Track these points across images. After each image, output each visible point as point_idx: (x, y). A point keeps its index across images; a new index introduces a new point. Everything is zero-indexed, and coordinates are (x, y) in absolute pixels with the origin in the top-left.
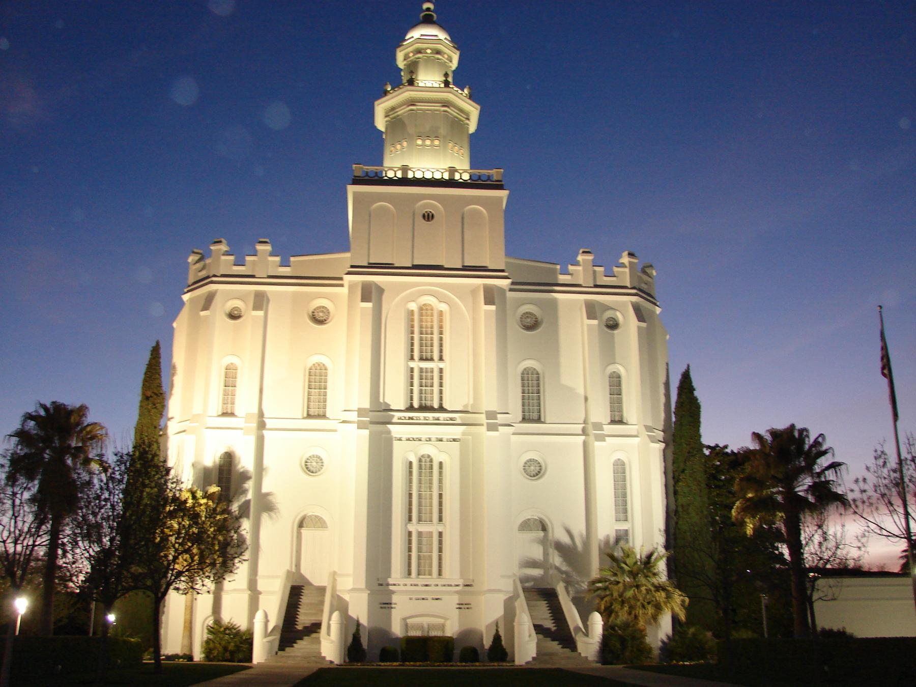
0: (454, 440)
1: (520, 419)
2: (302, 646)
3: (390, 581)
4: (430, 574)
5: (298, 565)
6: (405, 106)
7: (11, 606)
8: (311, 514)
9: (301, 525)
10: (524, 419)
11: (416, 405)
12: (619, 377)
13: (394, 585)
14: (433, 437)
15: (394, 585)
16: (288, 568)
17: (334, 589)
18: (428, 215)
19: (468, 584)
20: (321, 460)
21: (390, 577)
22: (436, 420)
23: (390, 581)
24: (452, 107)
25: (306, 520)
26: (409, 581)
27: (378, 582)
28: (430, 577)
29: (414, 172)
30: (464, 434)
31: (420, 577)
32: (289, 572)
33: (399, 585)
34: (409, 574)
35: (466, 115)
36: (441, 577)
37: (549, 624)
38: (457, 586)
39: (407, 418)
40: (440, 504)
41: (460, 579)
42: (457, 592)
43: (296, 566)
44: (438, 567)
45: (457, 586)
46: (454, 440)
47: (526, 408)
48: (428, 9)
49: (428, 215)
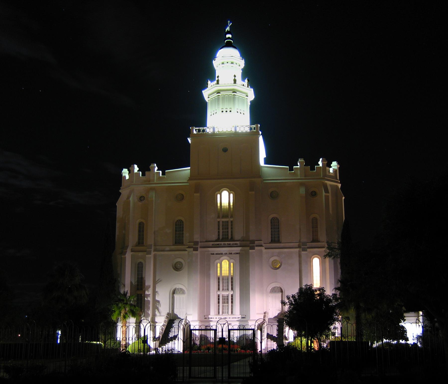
0: (237, 253)
1: (270, 240)
2: (169, 345)
3: (210, 316)
4: (228, 313)
5: (173, 310)
6: (216, 93)
7: (341, 286)
8: (178, 287)
9: (174, 293)
10: (272, 241)
11: (221, 237)
12: (317, 220)
13: (211, 318)
14: (228, 253)
15: (211, 318)
16: (168, 311)
17: (186, 320)
18: (225, 149)
19: (243, 317)
20: (315, 192)
21: (210, 315)
22: (229, 245)
23: (210, 316)
24: (238, 92)
25: (176, 290)
26: (218, 317)
27: (205, 317)
28: (227, 314)
29: (218, 129)
30: (241, 250)
31: (223, 314)
32: (168, 314)
33: (213, 318)
34: (219, 313)
35: (246, 94)
36: (232, 314)
37: (275, 334)
38: (238, 318)
39: (216, 245)
40: (219, 285)
41: (240, 315)
42: (238, 321)
43: (172, 311)
44: (222, 310)
45: (238, 318)
46: (237, 253)
47: (273, 236)
48: (229, 38)
49: (225, 149)
